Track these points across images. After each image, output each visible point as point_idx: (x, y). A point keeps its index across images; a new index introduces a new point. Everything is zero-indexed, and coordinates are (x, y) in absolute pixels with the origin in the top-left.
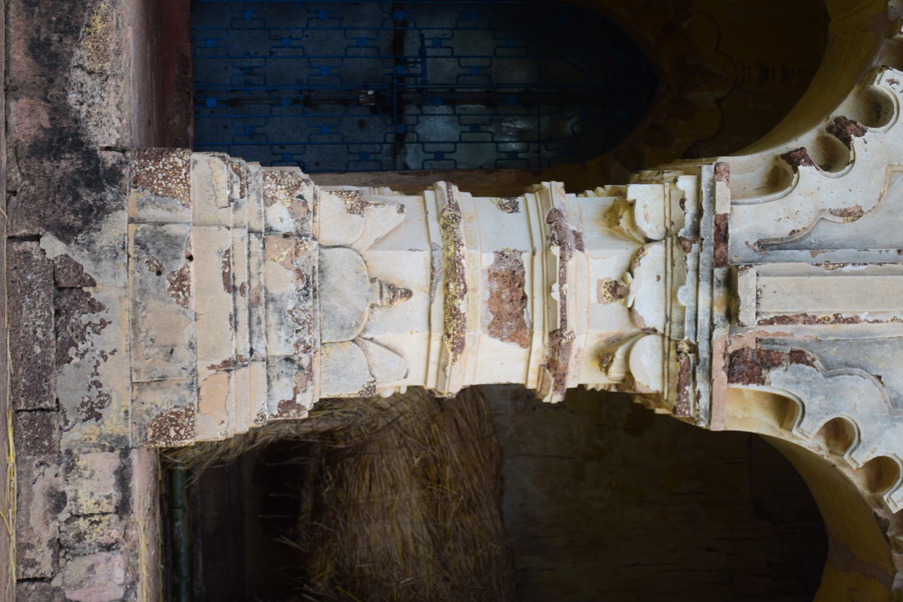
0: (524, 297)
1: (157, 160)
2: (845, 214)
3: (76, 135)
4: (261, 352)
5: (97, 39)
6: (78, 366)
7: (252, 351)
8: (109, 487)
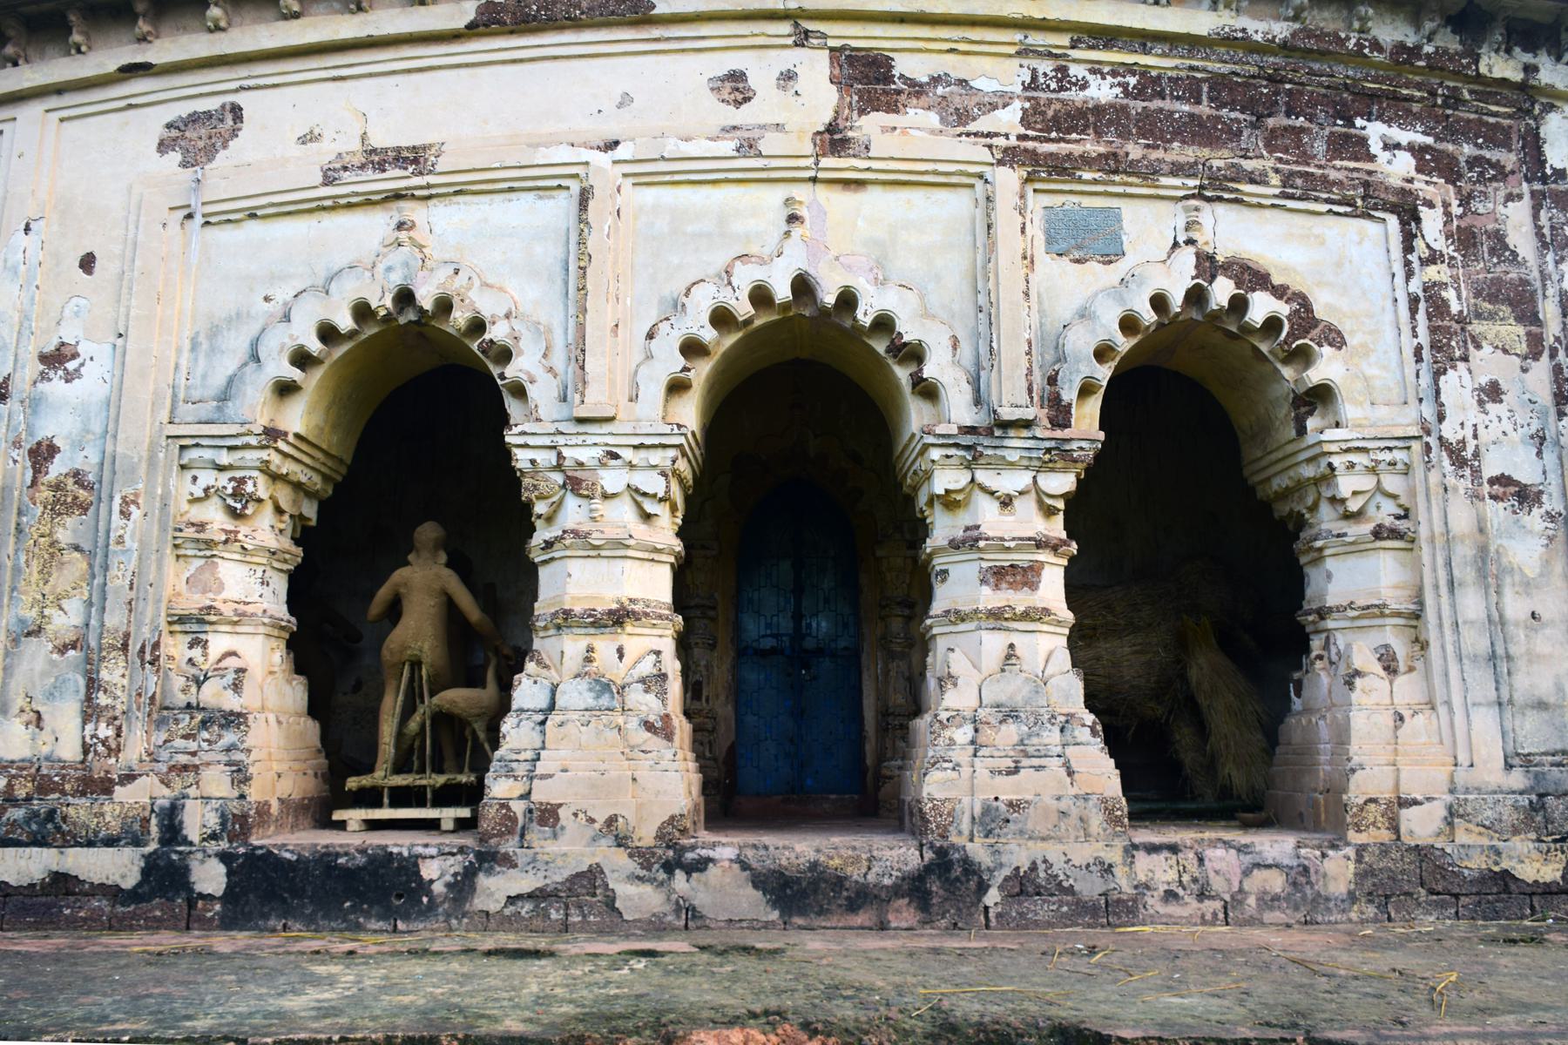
0: (1012, 566)
1: (929, 821)
2: (955, 347)
3: (913, 879)
4: (1059, 750)
5: (846, 864)
6: (1075, 880)
7: (1059, 756)
8: (1159, 859)
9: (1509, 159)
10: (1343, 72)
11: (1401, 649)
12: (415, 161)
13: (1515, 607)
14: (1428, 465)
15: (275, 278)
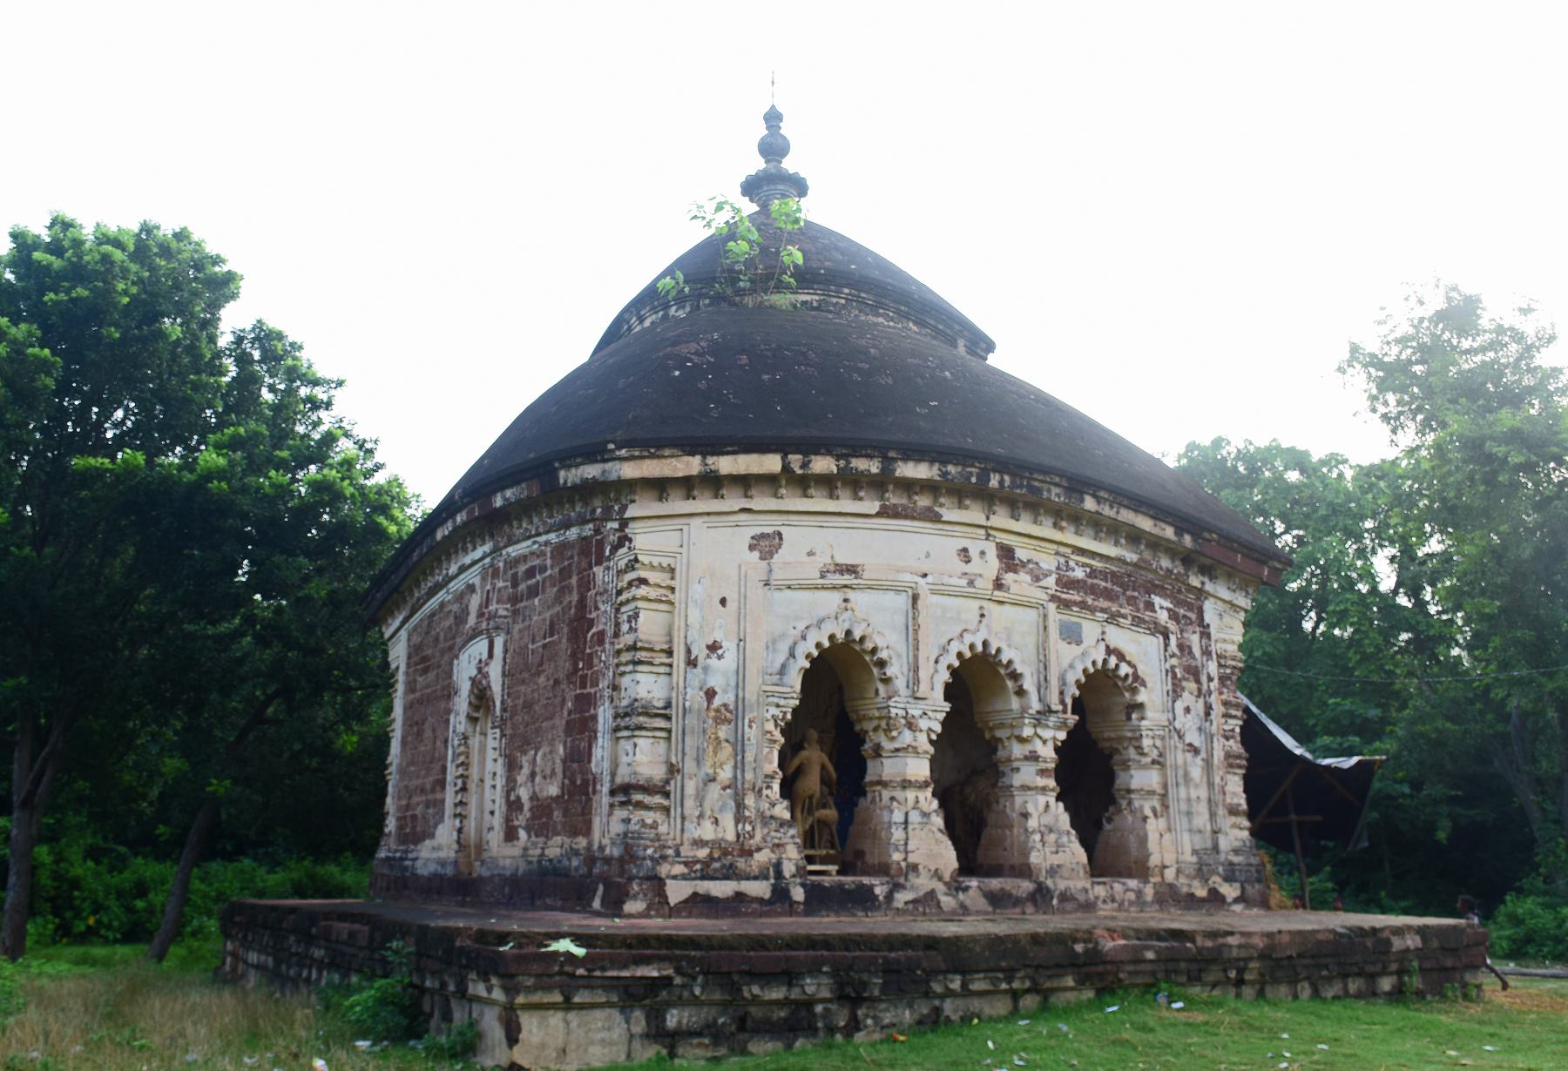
10: (1150, 576)
11: (1159, 808)
12: (855, 572)
13: (1193, 794)
14: (1170, 737)
15: (797, 618)
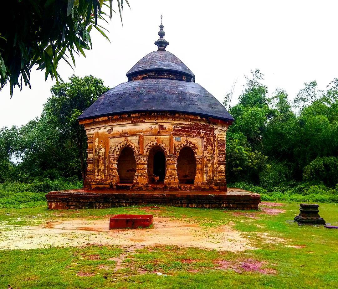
9: (212, 133)
13: (208, 169)
15: (116, 143)
